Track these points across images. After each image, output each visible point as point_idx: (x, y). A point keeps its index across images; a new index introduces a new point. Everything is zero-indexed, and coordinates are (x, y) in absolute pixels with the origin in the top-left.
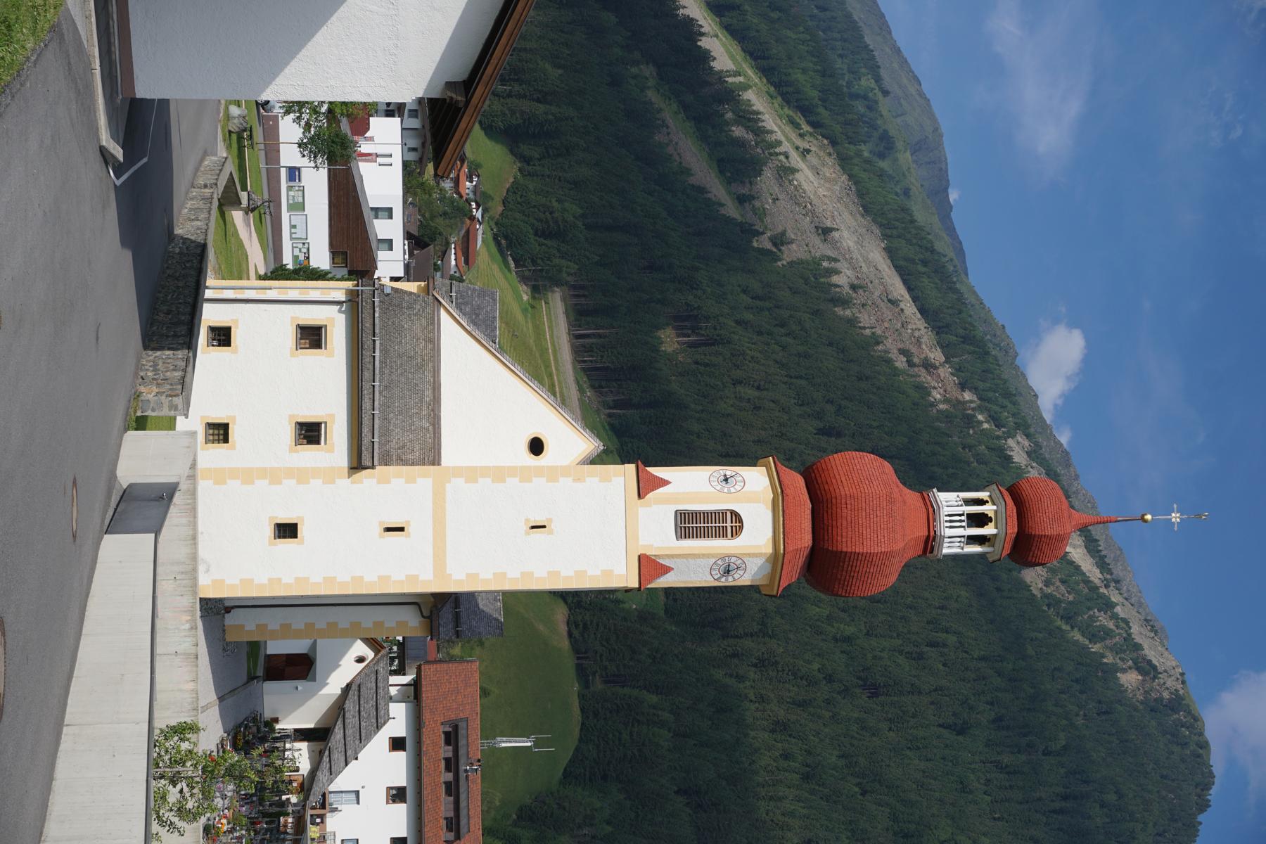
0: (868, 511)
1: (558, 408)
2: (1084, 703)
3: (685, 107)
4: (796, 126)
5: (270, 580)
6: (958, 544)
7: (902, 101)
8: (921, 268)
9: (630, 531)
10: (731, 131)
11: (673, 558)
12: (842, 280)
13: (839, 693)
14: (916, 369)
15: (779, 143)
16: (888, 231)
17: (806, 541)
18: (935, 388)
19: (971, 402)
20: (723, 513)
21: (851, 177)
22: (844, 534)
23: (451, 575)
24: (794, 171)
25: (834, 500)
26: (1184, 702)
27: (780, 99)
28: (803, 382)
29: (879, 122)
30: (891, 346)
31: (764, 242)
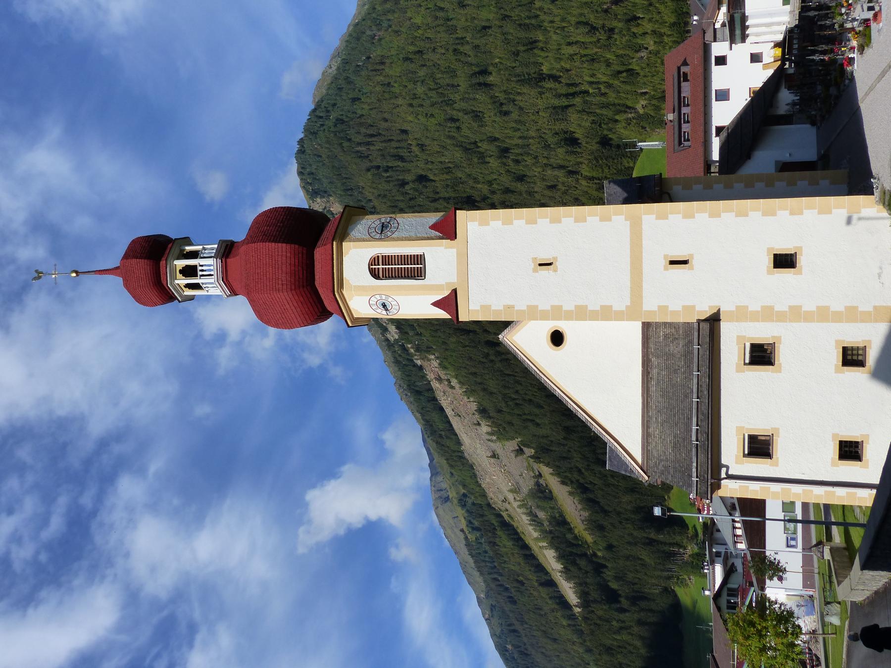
0: (265, 278)
1: (538, 372)
2: (359, 195)
3: (571, 530)
4: (510, 516)
5: (801, 213)
6: (206, 252)
7: (454, 526)
8: (443, 433)
9: (463, 260)
10: (545, 515)
11: (428, 237)
12: (485, 428)
13: (488, 198)
14: (446, 378)
15: (519, 507)
16: (460, 455)
17: (318, 253)
18: (436, 367)
19: (417, 359)
20: (386, 277)
21: (480, 486)
22: (284, 258)
23: (626, 220)
24: (511, 491)
25: (293, 287)
26: (309, 196)
27: (519, 531)
28: (507, 372)
29: (466, 515)
30: (459, 390)
31: (529, 452)
